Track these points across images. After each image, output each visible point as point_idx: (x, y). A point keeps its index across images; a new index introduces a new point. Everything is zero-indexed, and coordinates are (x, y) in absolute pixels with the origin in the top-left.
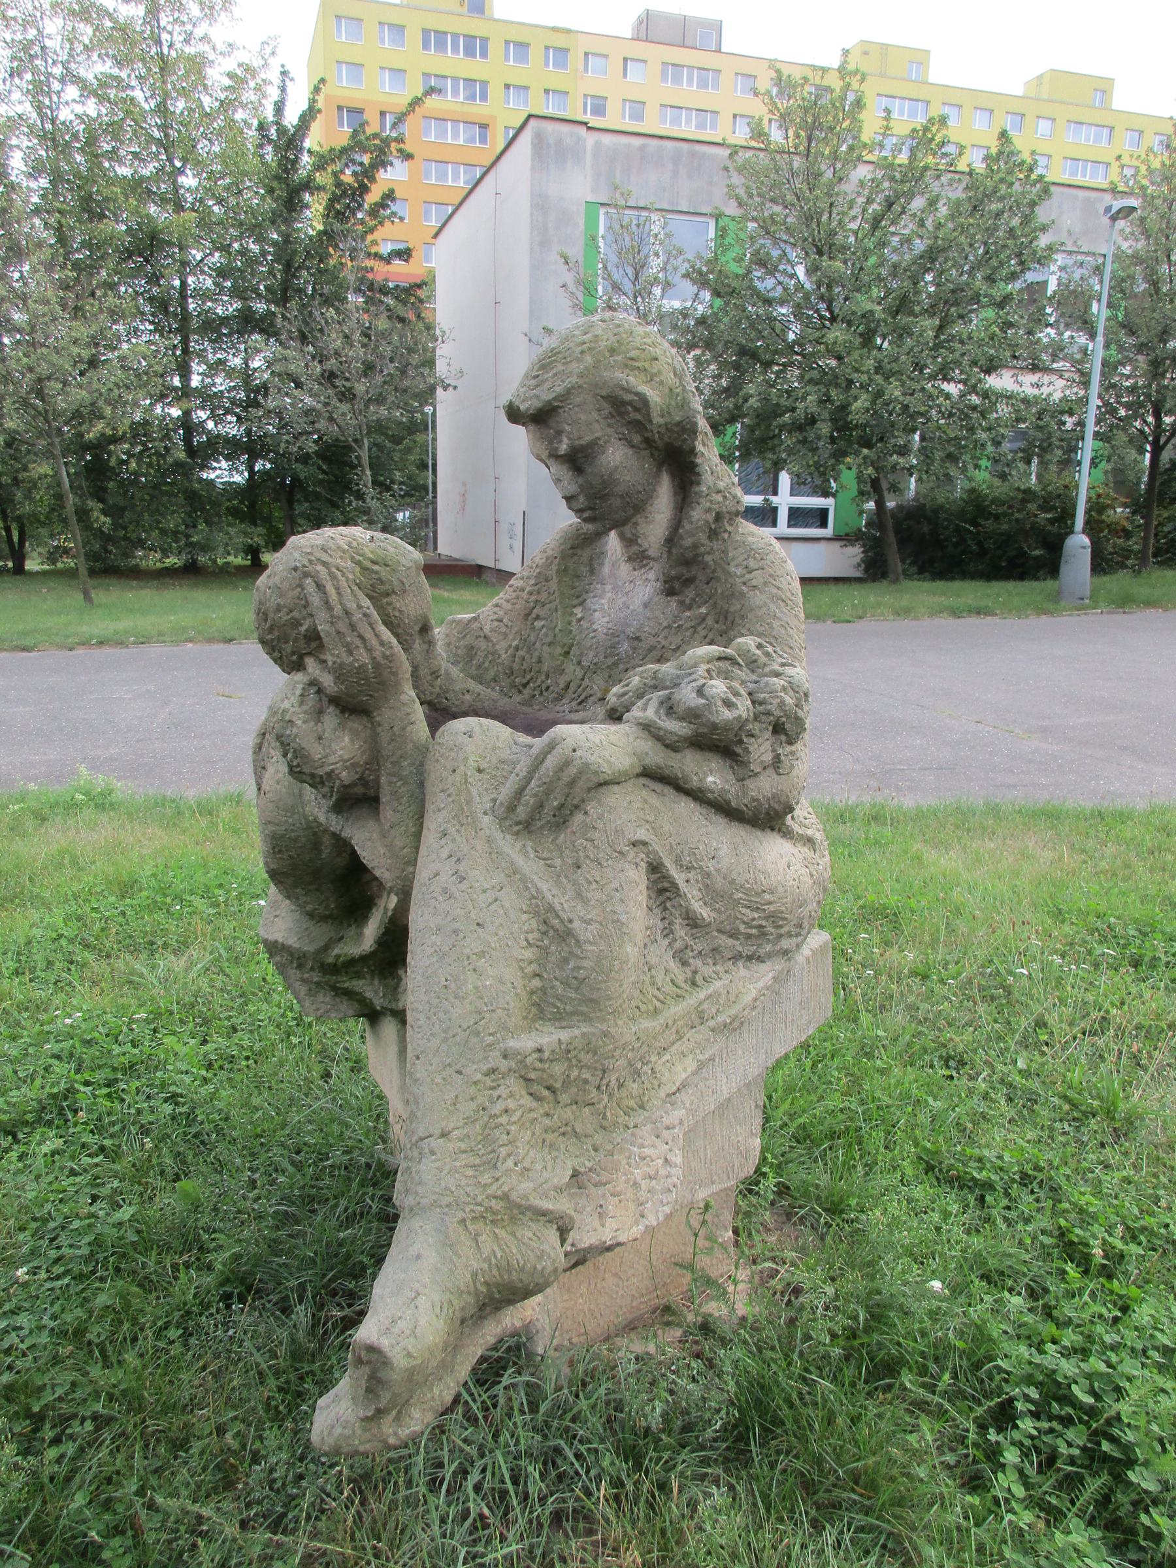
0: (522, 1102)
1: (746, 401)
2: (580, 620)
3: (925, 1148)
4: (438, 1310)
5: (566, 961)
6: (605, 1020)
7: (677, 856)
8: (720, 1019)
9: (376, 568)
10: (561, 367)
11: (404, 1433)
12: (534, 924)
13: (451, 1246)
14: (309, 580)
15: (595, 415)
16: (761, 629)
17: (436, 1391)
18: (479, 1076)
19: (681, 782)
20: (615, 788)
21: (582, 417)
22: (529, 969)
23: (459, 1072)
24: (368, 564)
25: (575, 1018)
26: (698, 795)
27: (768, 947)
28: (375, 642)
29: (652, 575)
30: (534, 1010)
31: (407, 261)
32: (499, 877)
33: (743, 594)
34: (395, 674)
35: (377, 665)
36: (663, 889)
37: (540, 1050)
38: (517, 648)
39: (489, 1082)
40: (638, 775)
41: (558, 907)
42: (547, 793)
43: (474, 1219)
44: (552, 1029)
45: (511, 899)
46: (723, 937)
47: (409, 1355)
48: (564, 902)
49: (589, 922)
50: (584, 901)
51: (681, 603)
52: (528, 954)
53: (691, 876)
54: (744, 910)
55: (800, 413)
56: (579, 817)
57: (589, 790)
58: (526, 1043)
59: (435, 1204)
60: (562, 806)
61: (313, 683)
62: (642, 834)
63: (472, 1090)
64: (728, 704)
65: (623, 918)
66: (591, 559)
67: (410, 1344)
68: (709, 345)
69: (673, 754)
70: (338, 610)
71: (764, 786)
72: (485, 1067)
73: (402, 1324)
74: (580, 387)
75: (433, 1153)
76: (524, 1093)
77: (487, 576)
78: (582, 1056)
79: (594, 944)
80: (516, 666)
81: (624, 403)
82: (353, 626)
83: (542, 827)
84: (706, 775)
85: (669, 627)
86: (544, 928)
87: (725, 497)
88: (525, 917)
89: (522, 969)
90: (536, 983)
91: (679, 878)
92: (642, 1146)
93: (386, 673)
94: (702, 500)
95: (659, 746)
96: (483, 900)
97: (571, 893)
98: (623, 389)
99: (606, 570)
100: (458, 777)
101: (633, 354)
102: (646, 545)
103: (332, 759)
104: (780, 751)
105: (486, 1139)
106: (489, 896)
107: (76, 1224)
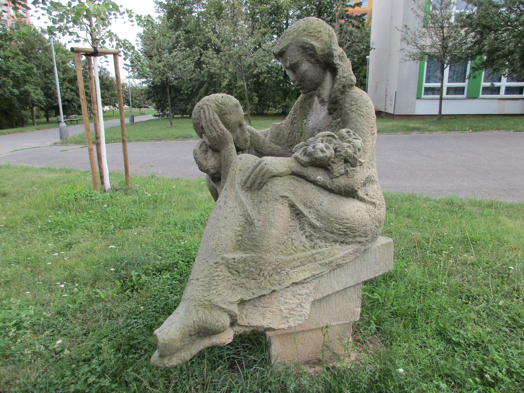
0: (225, 274)
1: (483, 47)
2: (305, 124)
3: (440, 326)
4: (178, 329)
5: (250, 232)
6: (260, 253)
7: (304, 203)
8: (323, 261)
9: (221, 106)
10: (286, 37)
11: (171, 364)
12: (243, 219)
13: (189, 312)
14: (202, 110)
15: (297, 53)
16: (353, 126)
17: (183, 354)
18: (212, 264)
19: (307, 178)
20: (279, 178)
21: (293, 54)
22: (238, 233)
23: (207, 262)
24: (219, 105)
25: (250, 251)
26: (314, 183)
27: (351, 240)
28: (218, 129)
29: (326, 108)
30: (238, 246)
31: (360, 7)
32: (236, 204)
33: (349, 114)
34: (226, 139)
35: (219, 136)
36: (297, 213)
37: (234, 259)
38: (289, 133)
39: (215, 266)
40: (290, 174)
41: (251, 215)
42: (256, 178)
43: (198, 305)
44: (241, 253)
45: (238, 211)
46: (328, 233)
47: (164, 339)
48: (254, 214)
49: (259, 221)
50: (260, 213)
51: (333, 117)
52: (239, 229)
53: (311, 210)
54: (335, 225)
55: (506, 51)
56: (265, 186)
57: (269, 178)
58: (230, 256)
59: (188, 299)
60: (261, 183)
61: (204, 142)
62: (286, 194)
63: (209, 268)
64: (322, 151)
65: (272, 221)
66: (310, 103)
67: (165, 337)
68: (470, 25)
69: (304, 168)
70: (208, 119)
71: (342, 181)
72: (215, 261)
73: (165, 330)
74: (292, 44)
75: (193, 284)
76: (227, 271)
77: (383, 115)
78: (250, 263)
79: (260, 228)
80: (289, 139)
81: (307, 48)
82: (212, 124)
83: (255, 189)
84: (317, 176)
85: (328, 126)
86: (246, 221)
87: (347, 79)
88: (241, 217)
89: (235, 233)
90: (240, 238)
91: (305, 211)
92: (286, 298)
93: (222, 139)
94: (337, 81)
95: (299, 165)
96: (229, 210)
97: (256, 211)
98: (305, 43)
99: (314, 106)
100: (234, 172)
101: (311, 31)
102: (323, 97)
103: (208, 165)
104: (348, 169)
105: (209, 283)
106: (232, 209)
107: (163, 298)
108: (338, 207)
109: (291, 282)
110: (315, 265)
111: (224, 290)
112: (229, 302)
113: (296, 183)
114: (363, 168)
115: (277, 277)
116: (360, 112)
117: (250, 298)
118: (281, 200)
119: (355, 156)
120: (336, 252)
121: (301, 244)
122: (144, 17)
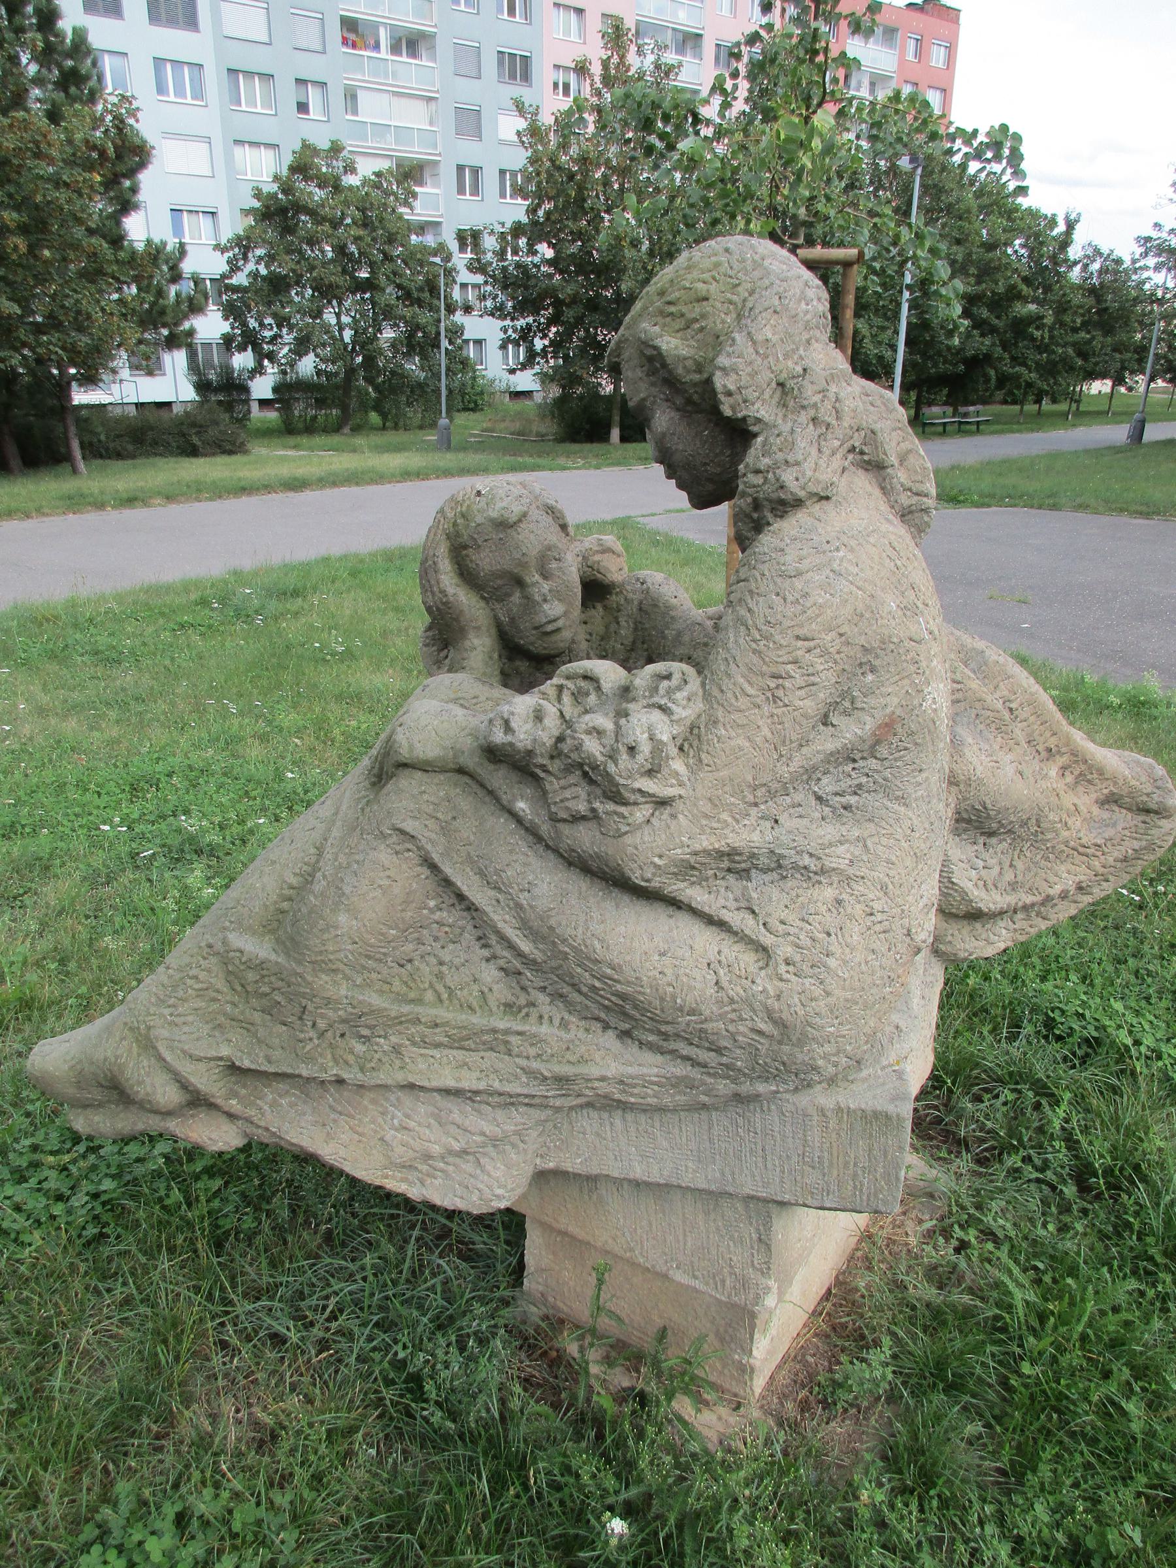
22: (286, 892)
30: (275, 924)
62: (409, 826)
65: (347, 890)
92: (408, 1116)
104: (597, 805)
108: (582, 918)
109: (400, 1077)
110: (505, 1064)
111: (190, 1019)
112: (184, 1052)
113: (465, 803)
114: (673, 816)
115: (360, 1048)
116: (743, 612)
117: (253, 1067)
118: (395, 839)
119: (612, 768)
120: (597, 1056)
121: (476, 987)
122: (988, 134)
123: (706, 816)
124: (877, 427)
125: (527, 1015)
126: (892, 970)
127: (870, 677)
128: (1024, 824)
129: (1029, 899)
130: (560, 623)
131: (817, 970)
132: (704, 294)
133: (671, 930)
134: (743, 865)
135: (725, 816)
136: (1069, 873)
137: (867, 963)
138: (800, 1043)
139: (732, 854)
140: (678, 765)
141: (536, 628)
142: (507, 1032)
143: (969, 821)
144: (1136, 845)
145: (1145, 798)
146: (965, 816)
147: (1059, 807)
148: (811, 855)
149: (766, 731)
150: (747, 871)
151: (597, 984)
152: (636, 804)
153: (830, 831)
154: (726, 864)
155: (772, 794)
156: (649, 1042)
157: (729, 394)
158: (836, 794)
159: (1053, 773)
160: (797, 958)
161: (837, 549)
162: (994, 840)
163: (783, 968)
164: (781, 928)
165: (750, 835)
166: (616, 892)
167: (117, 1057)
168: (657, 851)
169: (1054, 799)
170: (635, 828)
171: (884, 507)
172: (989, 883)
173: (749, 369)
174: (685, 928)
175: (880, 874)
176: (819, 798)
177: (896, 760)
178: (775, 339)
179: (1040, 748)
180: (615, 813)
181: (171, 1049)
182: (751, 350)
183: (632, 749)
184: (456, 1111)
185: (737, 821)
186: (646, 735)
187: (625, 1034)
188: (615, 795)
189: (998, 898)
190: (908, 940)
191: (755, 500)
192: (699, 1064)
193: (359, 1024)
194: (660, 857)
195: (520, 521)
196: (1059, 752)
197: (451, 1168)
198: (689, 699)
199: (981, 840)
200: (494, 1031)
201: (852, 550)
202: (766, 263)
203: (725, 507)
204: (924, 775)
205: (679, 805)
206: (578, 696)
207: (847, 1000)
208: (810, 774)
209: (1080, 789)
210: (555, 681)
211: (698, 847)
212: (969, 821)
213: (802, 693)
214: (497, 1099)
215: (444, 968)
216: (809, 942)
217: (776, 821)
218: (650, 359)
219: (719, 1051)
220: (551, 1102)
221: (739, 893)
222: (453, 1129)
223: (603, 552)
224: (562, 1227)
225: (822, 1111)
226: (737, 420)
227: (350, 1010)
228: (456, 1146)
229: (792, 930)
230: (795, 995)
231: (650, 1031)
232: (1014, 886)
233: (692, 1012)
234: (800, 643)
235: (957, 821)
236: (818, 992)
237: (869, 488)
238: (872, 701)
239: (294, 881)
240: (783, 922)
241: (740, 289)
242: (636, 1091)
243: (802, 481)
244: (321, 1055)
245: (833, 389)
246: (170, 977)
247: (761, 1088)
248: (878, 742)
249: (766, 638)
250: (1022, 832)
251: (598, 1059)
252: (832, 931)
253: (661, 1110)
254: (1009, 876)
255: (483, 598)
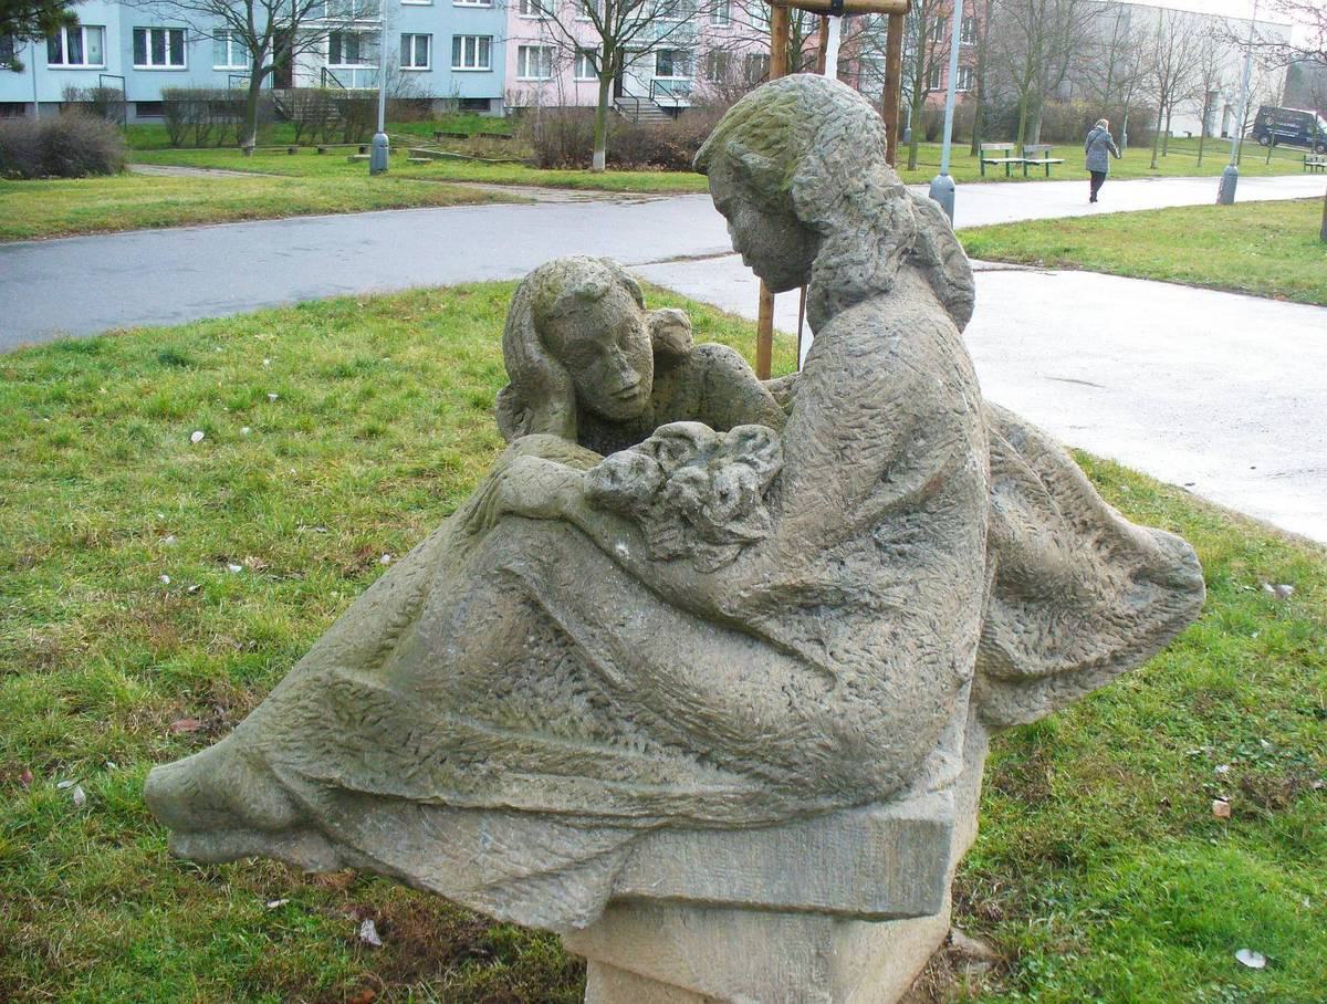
92: (499, 840)
110: (596, 787)
115: (459, 773)
123: (785, 556)
124: (926, 232)
125: (616, 742)
126: (938, 697)
127: (921, 442)
128: (1061, 590)
129: (1067, 664)
130: (637, 390)
131: (875, 692)
132: (785, 121)
133: (751, 659)
134: (814, 602)
135: (801, 556)
136: (1104, 641)
137: (917, 688)
138: (861, 758)
139: (801, 590)
140: (762, 511)
141: (613, 394)
142: (598, 756)
143: (1009, 584)
144: (1166, 617)
145: (1174, 574)
146: (1006, 578)
147: (1095, 578)
148: (871, 593)
149: (836, 485)
150: (816, 606)
151: (683, 708)
152: (726, 544)
153: (887, 574)
154: (799, 600)
155: (840, 541)
156: (728, 763)
157: (806, 204)
158: (894, 542)
159: (1089, 545)
160: (860, 681)
161: (895, 334)
162: (1033, 606)
163: (846, 691)
164: (846, 657)
165: (821, 574)
166: (703, 626)
167: (231, 780)
168: (744, 585)
169: (1089, 569)
170: (725, 565)
171: (933, 300)
172: (1030, 646)
173: (821, 185)
174: (763, 657)
175: (929, 613)
176: (878, 545)
177: (943, 514)
178: (843, 160)
179: (1076, 521)
180: (709, 552)
181: (286, 771)
182: (824, 170)
183: (724, 497)
184: (544, 833)
185: (811, 561)
186: (737, 484)
187: (703, 758)
188: (712, 537)
189: (1037, 661)
190: (952, 672)
191: (826, 291)
192: (771, 781)
193: (463, 751)
194: (745, 590)
195: (603, 295)
196: (1094, 526)
197: (536, 891)
198: (772, 456)
199: (1022, 605)
200: (585, 755)
201: (906, 336)
202: (834, 99)
203: (798, 291)
204: (967, 528)
205: (762, 546)
206: (673, 453)
207: (901, 720)
208: (871, 523)
209: (1115, 563)
210: (653, 438)
211: (777, 582)
212: (1009, 584)
213: (867, 453)
214: (584, 821)
215: (539, 700)
216: (869, 669)
217: (843, 563)
218: (737, 170)
219: (789, 767)
220: (635, 824)
221: (810, 627)
222: (541, 852)
223: (672, 325)
224: (627, 966)
225: (876, 823)
226: (812, 224)
227: (453, 736)
228: (544, 868)
229: (855, 658)
230: (854, 713)
231: (729, 752)
232: (1052, 651)
233: (768, 731)
234: (864, 411)
235: (999, 583)
236: (876, 711)
237: (920, 283)
238: (923, 462)
239: (397, 619)
240: (847, 651)
241: (814, 119)
242: (714, 809)
243: (866, 277)
244: (422, 779)
245: (890, 202)
246: (277, 709)
247: (825, 803)
248: (928, 498)
249: (837, 406)
250: (1059, 598)
251: (680, 780)
252: (889, 659)
253: (733, 828)
254: (1048, 641)
255: (564, 365)
